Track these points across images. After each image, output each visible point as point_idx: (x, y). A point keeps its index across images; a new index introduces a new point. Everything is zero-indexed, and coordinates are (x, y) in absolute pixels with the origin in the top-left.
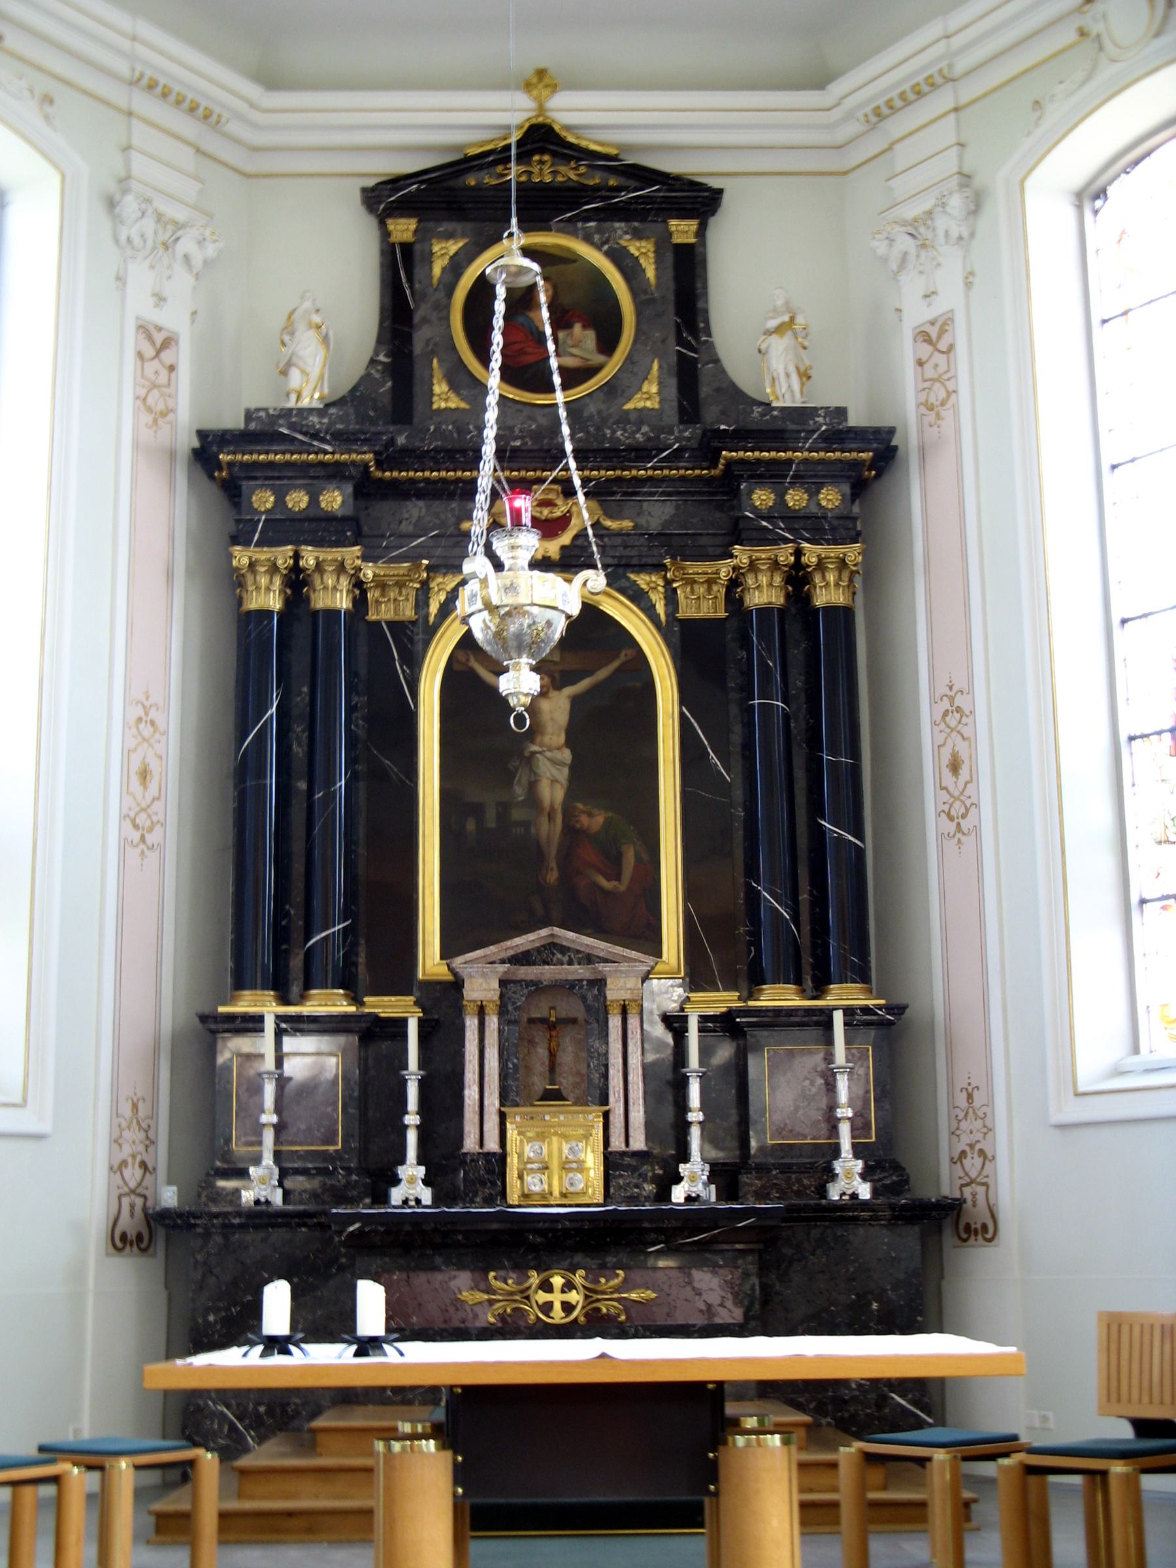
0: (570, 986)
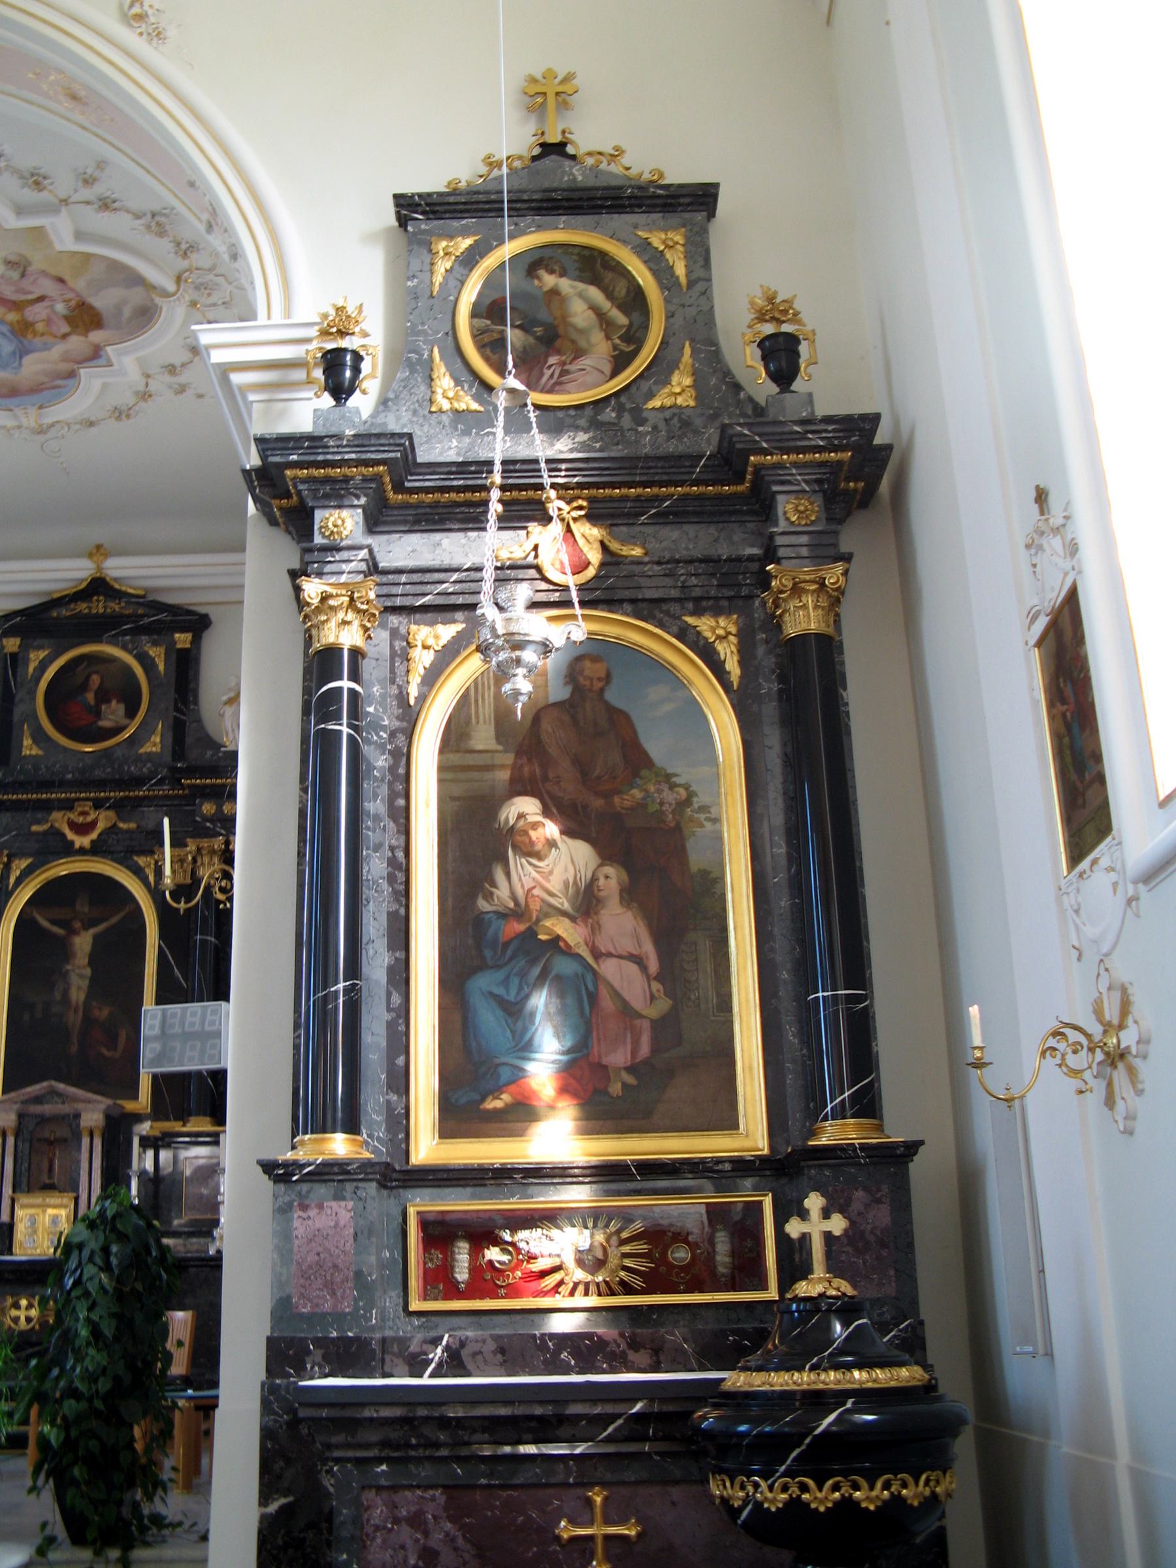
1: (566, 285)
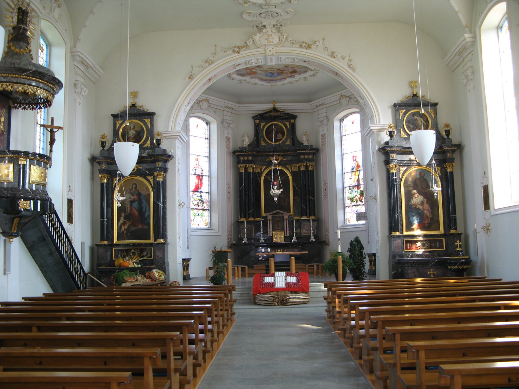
0: (280, 217)
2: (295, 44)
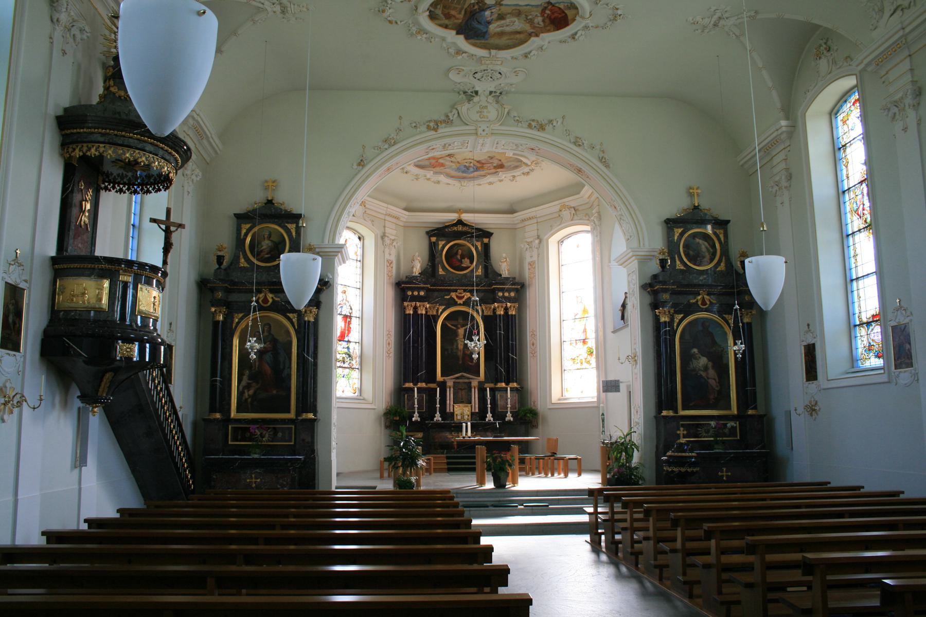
1: (701, 241)
2: (521, 122)
